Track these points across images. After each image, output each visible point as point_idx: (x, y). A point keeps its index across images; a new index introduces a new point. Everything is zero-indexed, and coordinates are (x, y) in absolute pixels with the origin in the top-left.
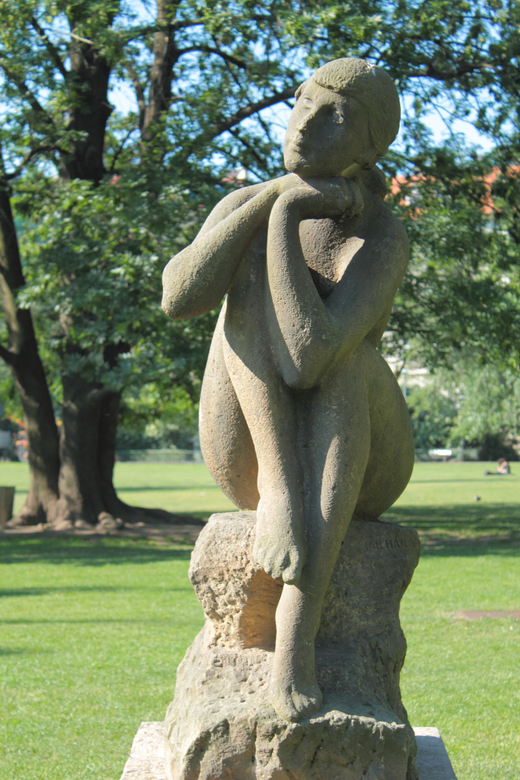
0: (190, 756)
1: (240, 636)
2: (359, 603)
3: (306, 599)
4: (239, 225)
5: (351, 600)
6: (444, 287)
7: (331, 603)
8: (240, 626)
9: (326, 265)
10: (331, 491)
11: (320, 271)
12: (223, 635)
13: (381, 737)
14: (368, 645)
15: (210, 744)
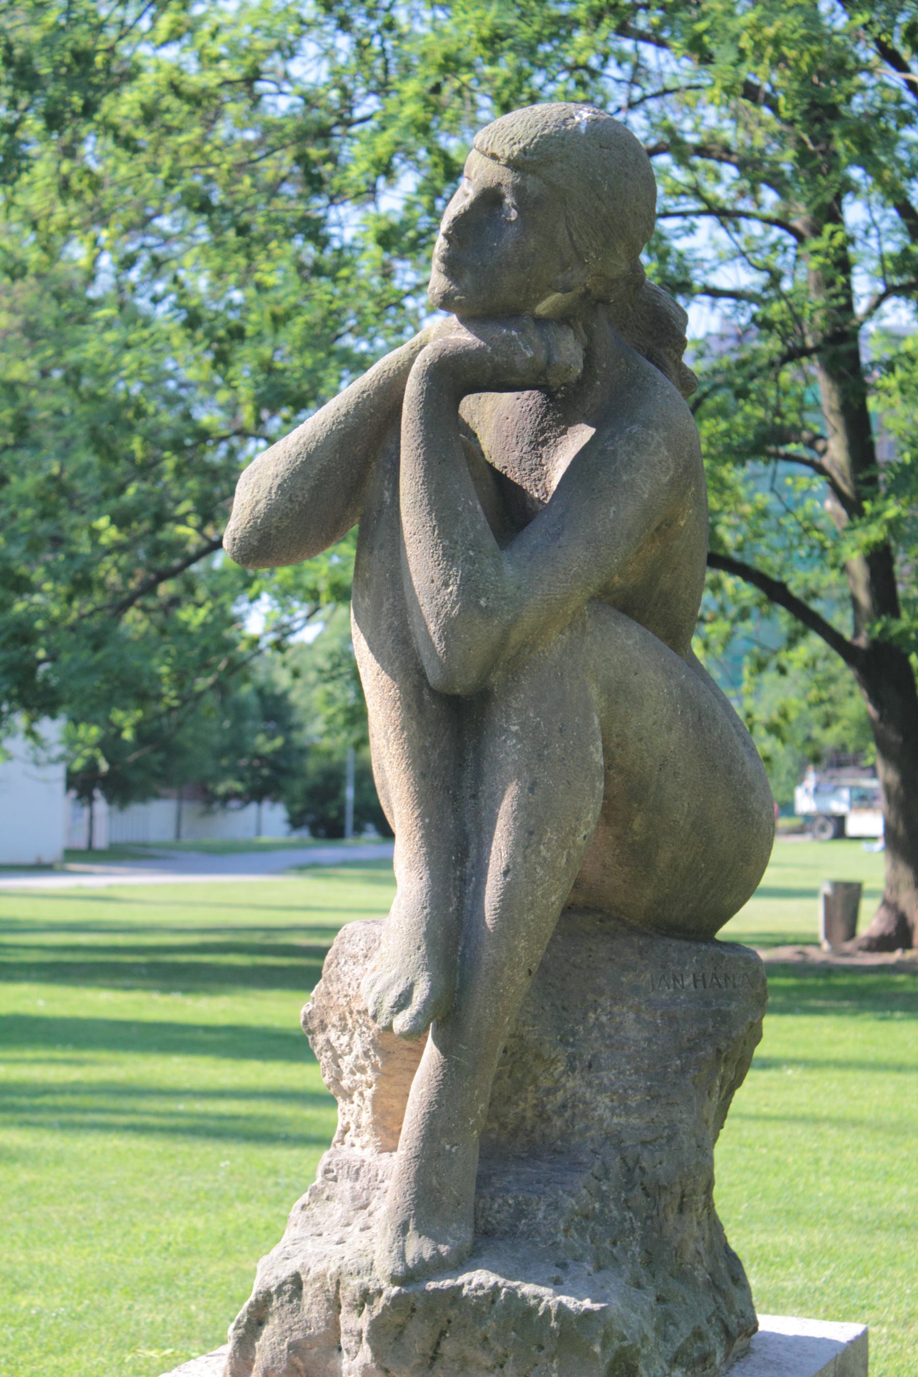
0: (240, 1331)
1: (375, 1130)
2: (612, 1084)
3: (449, 1068)
4: (358, 403)
5: (597, 1078)
7: (558, 1081)
8: (374, 1112)
9: (535, 474)
10: (500, 877)
11: (526, 485)
13: (554, 1324)
14: (618, 1159)
15: (272, 1314)
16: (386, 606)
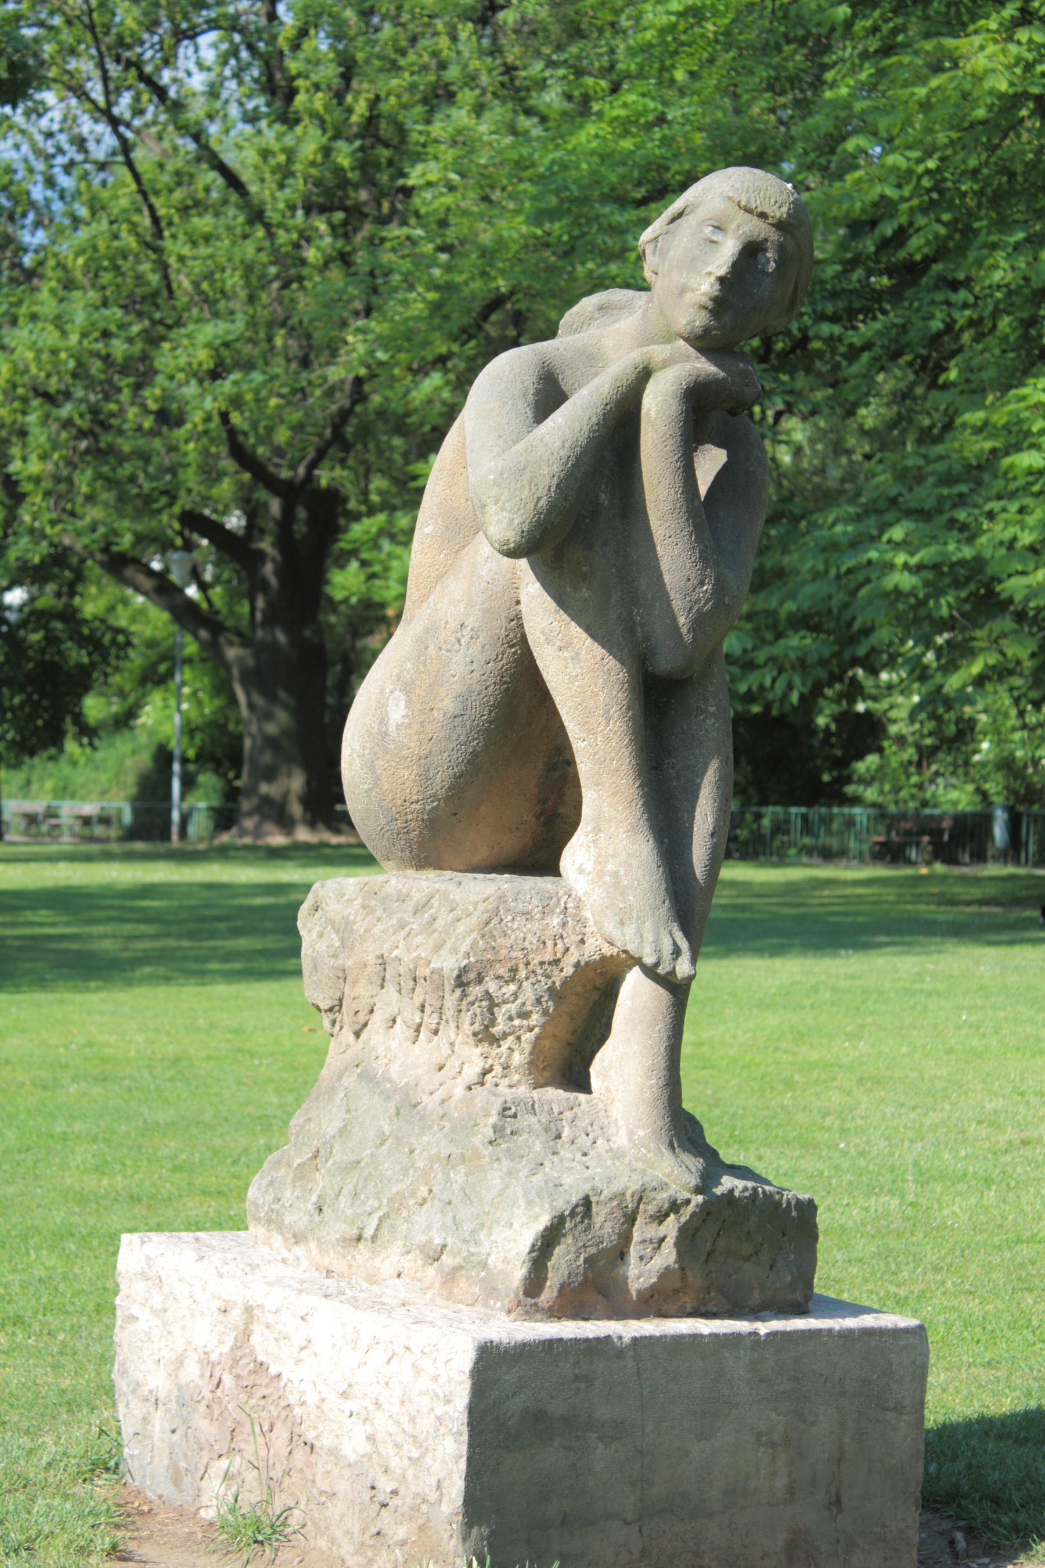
6: (168, 477)
12: (498, 1069)
13: (794, 1213)
16: (615, 599)
